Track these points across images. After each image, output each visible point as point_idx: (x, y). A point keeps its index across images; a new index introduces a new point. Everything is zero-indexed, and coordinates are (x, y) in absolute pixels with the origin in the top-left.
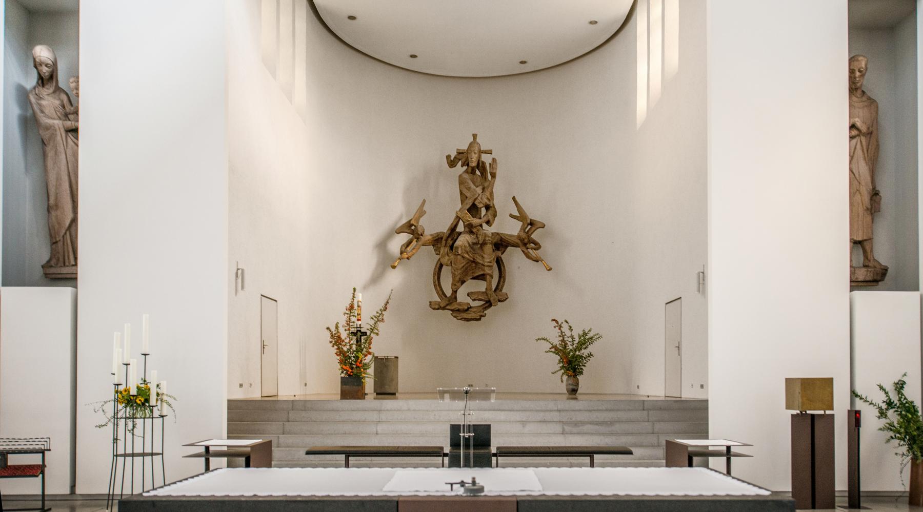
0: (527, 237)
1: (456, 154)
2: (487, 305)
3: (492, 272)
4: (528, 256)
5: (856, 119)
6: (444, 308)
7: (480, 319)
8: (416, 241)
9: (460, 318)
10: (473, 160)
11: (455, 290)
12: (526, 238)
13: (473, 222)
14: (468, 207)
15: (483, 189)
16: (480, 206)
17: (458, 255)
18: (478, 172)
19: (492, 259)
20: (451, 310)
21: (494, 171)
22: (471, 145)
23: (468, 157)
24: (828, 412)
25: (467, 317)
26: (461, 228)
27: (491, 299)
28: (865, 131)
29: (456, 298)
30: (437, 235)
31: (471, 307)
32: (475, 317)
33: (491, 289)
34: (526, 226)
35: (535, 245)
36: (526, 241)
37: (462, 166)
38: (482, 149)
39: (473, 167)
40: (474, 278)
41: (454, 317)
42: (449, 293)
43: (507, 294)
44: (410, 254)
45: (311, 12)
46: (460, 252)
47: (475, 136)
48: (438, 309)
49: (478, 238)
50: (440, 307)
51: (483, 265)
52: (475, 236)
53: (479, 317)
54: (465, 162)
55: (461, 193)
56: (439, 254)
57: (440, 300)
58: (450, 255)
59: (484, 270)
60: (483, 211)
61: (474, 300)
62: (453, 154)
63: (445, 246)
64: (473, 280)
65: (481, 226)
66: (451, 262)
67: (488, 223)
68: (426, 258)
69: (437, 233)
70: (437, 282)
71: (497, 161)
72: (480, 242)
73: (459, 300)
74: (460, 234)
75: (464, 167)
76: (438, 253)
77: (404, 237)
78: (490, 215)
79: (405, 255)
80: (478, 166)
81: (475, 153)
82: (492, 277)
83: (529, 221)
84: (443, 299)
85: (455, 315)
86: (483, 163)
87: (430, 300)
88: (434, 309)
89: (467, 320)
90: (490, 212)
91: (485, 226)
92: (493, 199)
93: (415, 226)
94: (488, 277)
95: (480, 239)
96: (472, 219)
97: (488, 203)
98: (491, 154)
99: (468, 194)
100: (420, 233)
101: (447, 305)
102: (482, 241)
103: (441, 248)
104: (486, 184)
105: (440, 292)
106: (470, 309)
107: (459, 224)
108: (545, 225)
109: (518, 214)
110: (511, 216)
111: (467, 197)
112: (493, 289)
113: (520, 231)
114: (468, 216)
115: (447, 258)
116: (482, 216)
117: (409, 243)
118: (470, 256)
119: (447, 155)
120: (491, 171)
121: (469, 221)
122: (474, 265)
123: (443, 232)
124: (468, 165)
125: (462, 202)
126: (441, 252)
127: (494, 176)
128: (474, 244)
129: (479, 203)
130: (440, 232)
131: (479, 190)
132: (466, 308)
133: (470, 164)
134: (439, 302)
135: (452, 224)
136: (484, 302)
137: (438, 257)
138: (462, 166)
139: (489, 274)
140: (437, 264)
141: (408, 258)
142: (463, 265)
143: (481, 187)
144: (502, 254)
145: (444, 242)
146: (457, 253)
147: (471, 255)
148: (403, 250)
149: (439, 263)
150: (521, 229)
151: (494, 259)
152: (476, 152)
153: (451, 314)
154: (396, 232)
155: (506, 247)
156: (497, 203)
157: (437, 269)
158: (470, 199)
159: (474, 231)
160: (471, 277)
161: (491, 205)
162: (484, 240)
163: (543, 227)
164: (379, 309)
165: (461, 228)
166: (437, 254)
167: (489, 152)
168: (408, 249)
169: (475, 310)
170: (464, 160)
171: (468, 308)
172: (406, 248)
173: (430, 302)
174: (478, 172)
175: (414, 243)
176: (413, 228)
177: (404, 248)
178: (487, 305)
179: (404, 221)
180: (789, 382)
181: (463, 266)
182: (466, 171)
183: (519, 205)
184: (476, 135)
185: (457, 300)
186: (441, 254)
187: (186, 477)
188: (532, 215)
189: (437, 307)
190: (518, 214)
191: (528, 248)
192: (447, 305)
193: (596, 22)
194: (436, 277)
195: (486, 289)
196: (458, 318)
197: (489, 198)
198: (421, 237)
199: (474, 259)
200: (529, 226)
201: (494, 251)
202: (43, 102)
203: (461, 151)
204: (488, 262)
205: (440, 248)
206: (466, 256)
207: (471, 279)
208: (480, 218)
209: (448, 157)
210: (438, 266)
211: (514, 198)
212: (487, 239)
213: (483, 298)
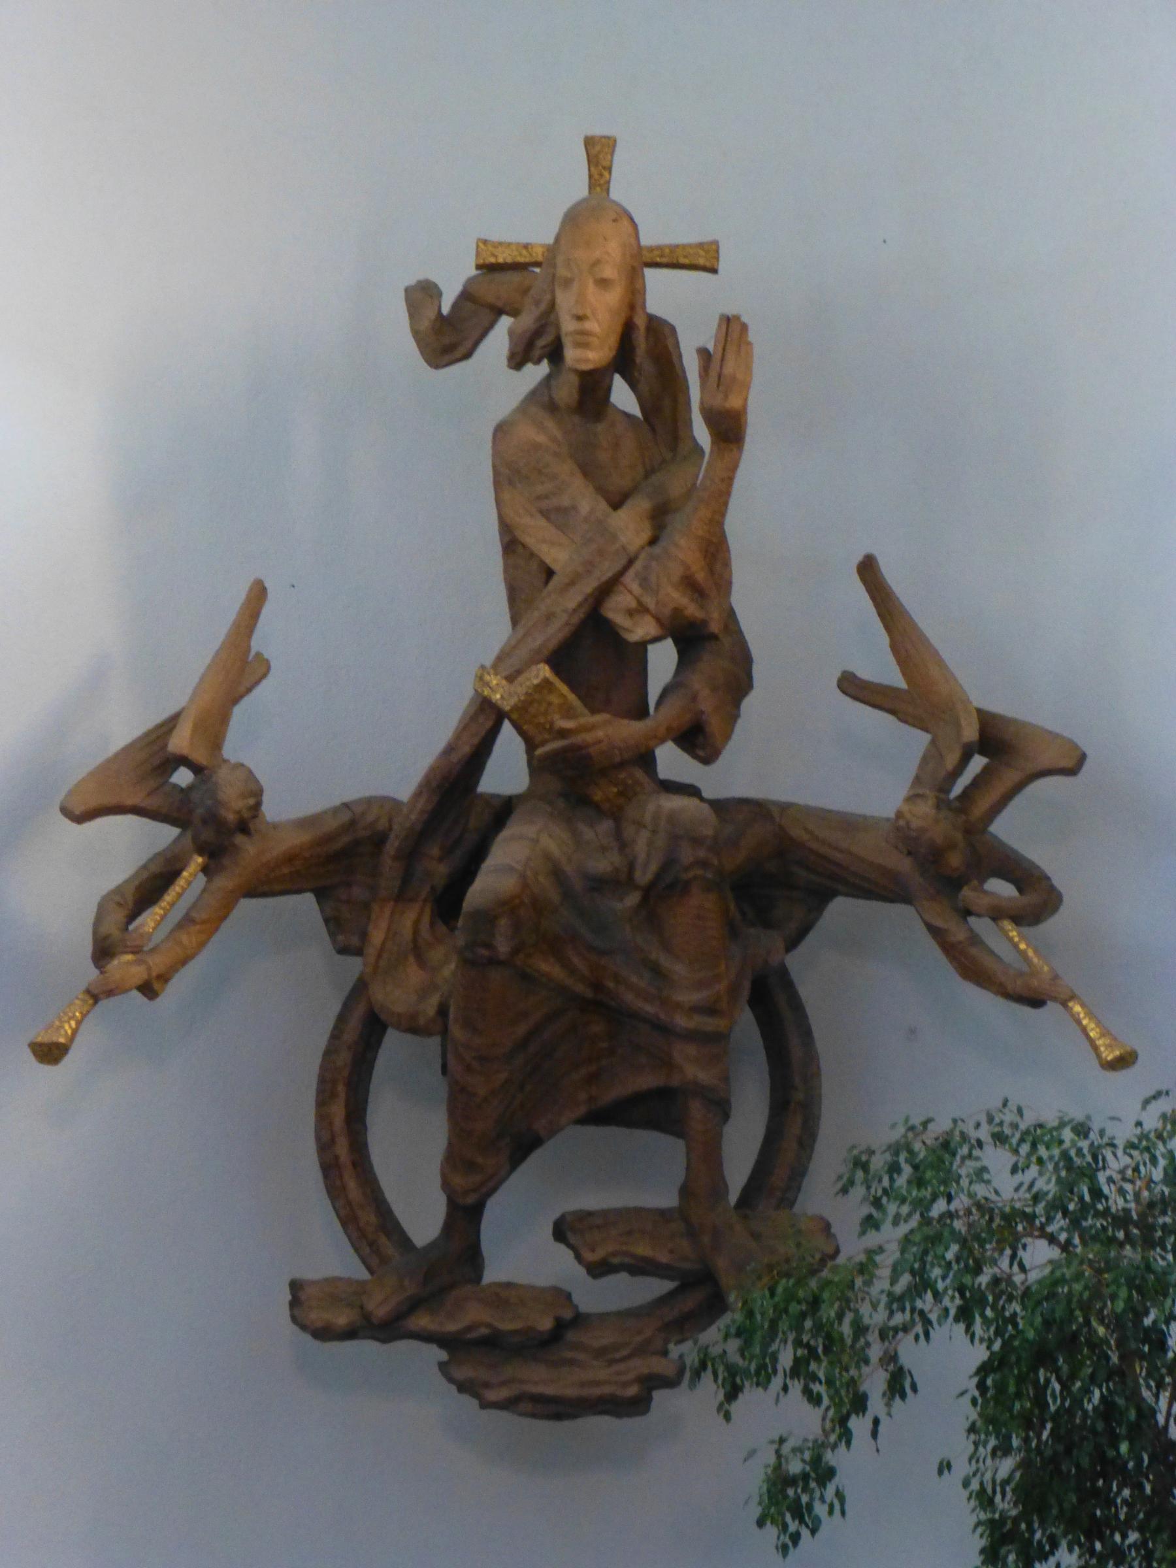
0: (959, 836)
1: (473, 272)
2: (690, 1302)
3: (726, 1079)
7: (638, 1405)
8: (205, 870)
9: (503, 1393)
10: (591, 325)
11: (471, 1200)
12: (952, 846)
13: (588, 737)
14: (553, 634)
15: (660, 517)
16: (639, 630)
17: (494, 962)
18: (623, 396)
19: (722, 986)
20: (442, 1341)
21: (734, 402)
22: (574, 219)
23: (552, 305)
25: (549, 1390)
27: (721, 1263)
28: (927, 1178)
29: (472, 1257)
30: (345, 817)
31: (579, 1320)
32: (607, 1390)
33: (719, 1188)
34: (951, 760)
35: (1020, 890)
36: (955, 860)
37: (518, 360)
38: (646, 240)
39: (591, 373)
40: (599, 1117)
41: (463, 1387)
43: (827, 1227)
44: (158, 963)
46: (503, 947)
48: (350, 1334)
49: (624, 846)
50: (366, 1316)
51: (664, 1029)
52: (607, 825)
53: (632, 1391)
54: (538, 333)
55: (511, 545)
56: (359, 952)
57: (363, 1274)
58: (436, 954)
59: (667, 1064)
61: (599, 1269)
63: (402, 897)
64: (591, 1131)
65: (647, 760)
66: (443, 1011)
69: (346, 805)
70: (342, 1149)
71: (752, 336)
72: (644, 876)
73: (492, 1274)
75: (529, 368)
76: (355, 941)
78: (705, 693)
79: (123, 965)
81: (603, 283)
82: (721, 1108)
83: (970, 732)
84: (384, 1260)
85: (464, 1372)
86: (660, 331)
87: (299, 1274)
88: (323, 1333)
90: (710, 664)
92: (724, 585)
93: (197, 769)
94: (696, 1109)
95: (641, 846)
96: (589, 719)
97: (692, 610)
98: (714, 271)
99: (558, 556)
100: (231, 817)
101: (414, 1305)
102: (653, 867)
103: (375, 907)
104: (675, 483)
105: (368, 1218)
106: (571, 1336)
108: (1082, 758)
109: (893, 677)
110: (852, 686)
111: (550, 573)
112: (733, 1197)
113: (911, 798)
114: (555, 699)
115: (414, 975)
116: (654, 691)
118: (572, 971)
119: (411, 281)
120: (717, 402)
121: (563, 733)
122: (598, 1028)
123: (383, 801)
124: (555, 354)
126: (377, 936)
128: (600, 884)
129: (631, 613)
130: (369, 801)
132: (546, 1324)
133: (571, 354)
134: (360, 1288)
135: (450, 749)
136: (668, 1286)
137: (354, 966)
138: (518, 360)
139: (699, 1090)
140: (342, 1019)
141: (148, 990)
142: (522, 1029)
143: (640, 505)
144: (792, 943)
145: (389, 865)
146: (484, 952)
147: (576, 960)
148: (116, 933)
149: (360, 1011)
150: (917, 780)
151: (733, 990)
152: (609, 272)
153: (443, 1366)
154: (66, 812)
155: (821, 897)
157: (344, 1058)
158: (572, 583)
159: (598, 796)
160: (582, 1110)
161: (715, 627)
162: (668, 864)
163: (1071, 771)
164: (1029, 1248)
166: (343, 950)
168: (149, 920)
169: (604, 1338)
170: (528, 320)
171: (561, 1326)
172: (133, 916)
173: (296, 1286)
174: (623, 396)
176: (183, 777)
177: (119, 916)
178: (690, 1302)
181: (524, 1043)
183: (905, 614)
185: (479, 1278)
186: (371, 952)
187: (1079, 1032)
189: (342, 1320)
190: (893, 677)
191: (967, 913)
192: (414, 1305)
194: (338, 1111)
195: (686, 1192)
196: (492, 1395)
197: (700, 576)
198: (239, 839)
199: (598, 987)
201: (733, 931)
203: (503, 257)
204: (696, 1009)
205: (366, 906)
206: (547, 967)
207: (583, 1121)
208: (640, 711)
210: (351, 1034)
211: (868, 570)
212: (687, 854)
213: (664, 1258)
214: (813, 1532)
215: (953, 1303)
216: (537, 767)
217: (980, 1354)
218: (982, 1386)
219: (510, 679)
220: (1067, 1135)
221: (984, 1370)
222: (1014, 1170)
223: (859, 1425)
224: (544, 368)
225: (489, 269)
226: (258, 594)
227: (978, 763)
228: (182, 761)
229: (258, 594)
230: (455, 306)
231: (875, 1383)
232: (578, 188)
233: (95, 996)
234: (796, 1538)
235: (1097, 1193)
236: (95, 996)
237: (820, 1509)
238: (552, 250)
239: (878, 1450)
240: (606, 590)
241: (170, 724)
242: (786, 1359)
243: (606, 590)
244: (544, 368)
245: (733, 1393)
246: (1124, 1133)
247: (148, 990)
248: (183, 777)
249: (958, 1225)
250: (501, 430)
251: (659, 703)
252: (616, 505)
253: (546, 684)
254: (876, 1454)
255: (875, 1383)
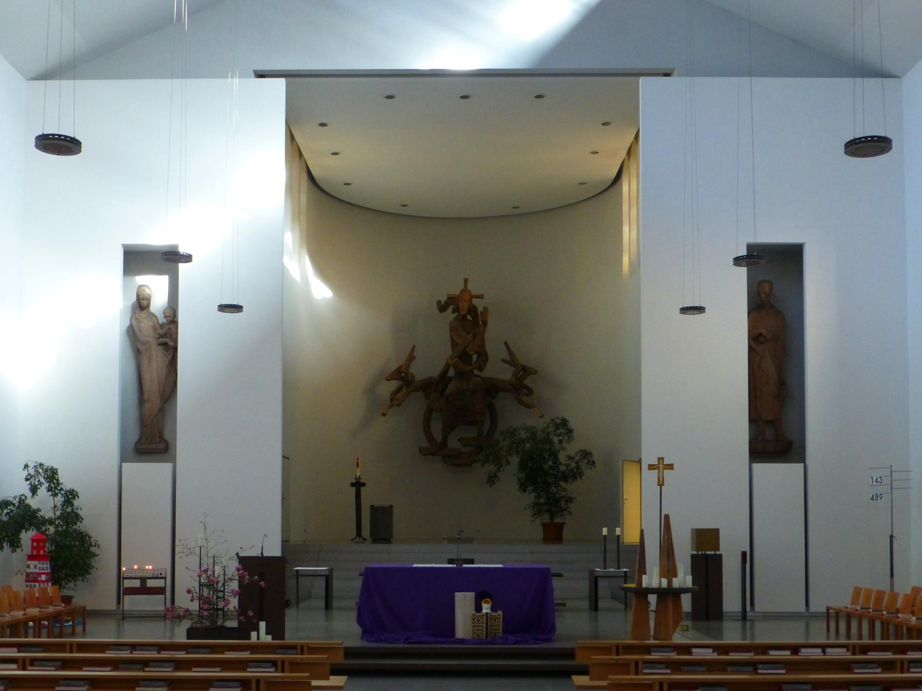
4: (520, 402)
5: (762, 330)
6: (433, 454)
18: (469, 317)
22: (462, 292)
24: (717, 553)
26: (451, 373)
42: (438, 437)
45: (312, 186)
47: (466, 281)
48: (428, 455)
55: (452, 340)
60: (475, 357)
61: (464, 446)
62: (444, 299)
65: (472, 372)
67: (480, 369)
68: (416, 404)
74: (451, 379)
77: (394, 384)
80: (469, 312)
86: (475, 308)
88: (424, 455)
89: (458, 465)
91: (476, 372)
107: (450, 371)
110: (504, 361)
117: (399, 390)
124: (459, 312)
125: (453, 348)
127: (485, 324)
131: (470, 337)
133: (461, 312)
138: (454, 312)
141: (398, 406)
156: (489, 347)
163: (535, 374)
165: (451, 373)
167: (481, 297)
168: (398, 396)
174: (469, 317)
175: (404, 389)
179: (394, 366)
180: (692, 529)
182: (456, 319)
184: (468, 279)
188: (523, 361)
193: (604, 124)
200: (522, 372)
202: (142, 325)
208: (471, 364)
209: (439, 302)
211: (506, 343)
214: (594, 468)
215: (515, 452)
216: (456, 373)
217: (519, 459)
218: (520, 464)
219: (452, 360)
220: (532, 429)
221: (519, 462)
222: (525, 433)
223: (502, 469)
224: (457, 314)
225: (449, 298)
226: (414, 347)
227: (522, 372)
228: (402, 372)
229: (414, 347)
230: (444, 304)
231: (504, 463)
232: (462, 287)
233: (390, 407)
234: (492, 485)
235: (536, 437)
236: (390, 407)
237: (496, 481)
238: (459, 295)
239: (187, 568)
240: (466, 347)
241: (401, 366)
242: (491, 460)
243: (466, 347)
244: (457, 314)
245: (483, 464)
246: (540, 428)
247: (398, 406)
248: (403, 374)
249: (516, 441)
250: (451, 323)
251: (475, 362)
252: (468, 334)
253: (457, 361)
254: (186, 566)
255: (504, 463)
